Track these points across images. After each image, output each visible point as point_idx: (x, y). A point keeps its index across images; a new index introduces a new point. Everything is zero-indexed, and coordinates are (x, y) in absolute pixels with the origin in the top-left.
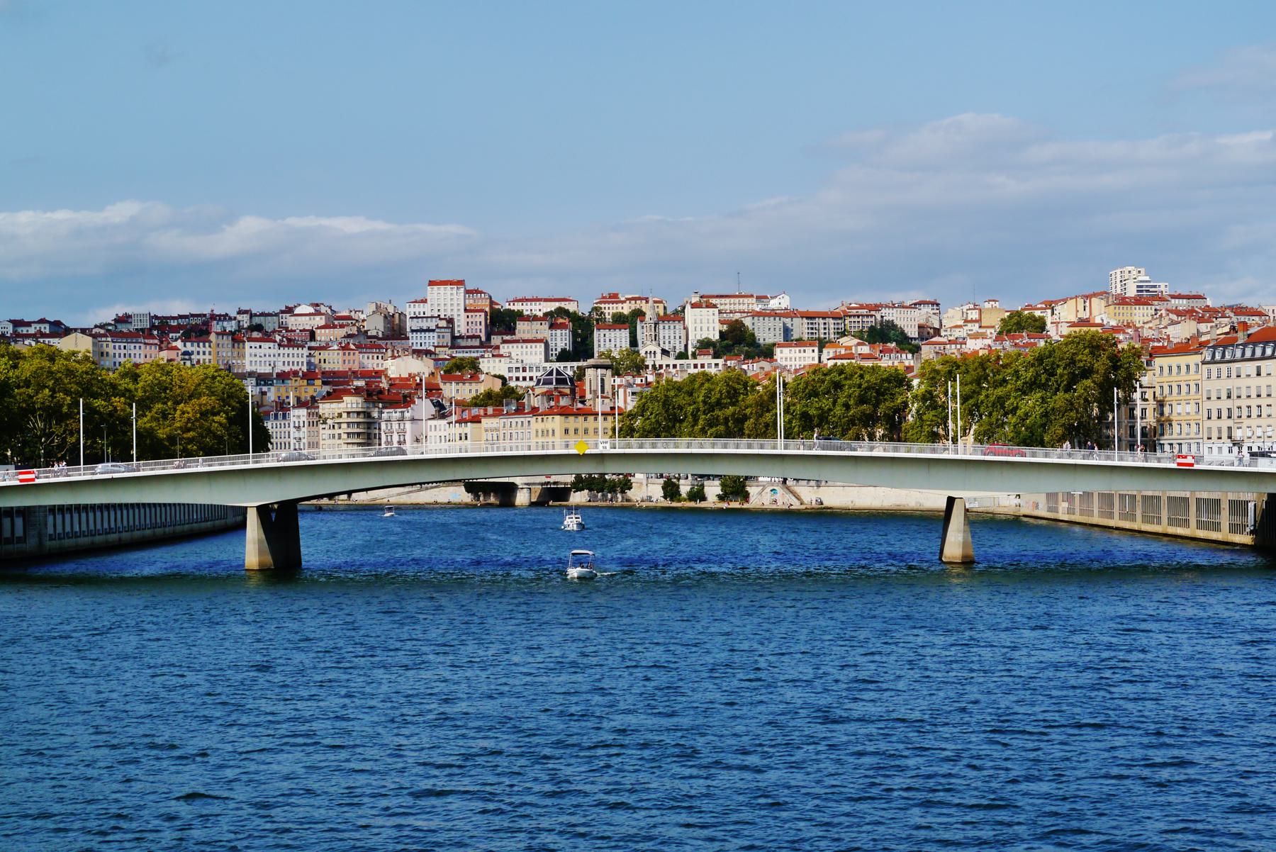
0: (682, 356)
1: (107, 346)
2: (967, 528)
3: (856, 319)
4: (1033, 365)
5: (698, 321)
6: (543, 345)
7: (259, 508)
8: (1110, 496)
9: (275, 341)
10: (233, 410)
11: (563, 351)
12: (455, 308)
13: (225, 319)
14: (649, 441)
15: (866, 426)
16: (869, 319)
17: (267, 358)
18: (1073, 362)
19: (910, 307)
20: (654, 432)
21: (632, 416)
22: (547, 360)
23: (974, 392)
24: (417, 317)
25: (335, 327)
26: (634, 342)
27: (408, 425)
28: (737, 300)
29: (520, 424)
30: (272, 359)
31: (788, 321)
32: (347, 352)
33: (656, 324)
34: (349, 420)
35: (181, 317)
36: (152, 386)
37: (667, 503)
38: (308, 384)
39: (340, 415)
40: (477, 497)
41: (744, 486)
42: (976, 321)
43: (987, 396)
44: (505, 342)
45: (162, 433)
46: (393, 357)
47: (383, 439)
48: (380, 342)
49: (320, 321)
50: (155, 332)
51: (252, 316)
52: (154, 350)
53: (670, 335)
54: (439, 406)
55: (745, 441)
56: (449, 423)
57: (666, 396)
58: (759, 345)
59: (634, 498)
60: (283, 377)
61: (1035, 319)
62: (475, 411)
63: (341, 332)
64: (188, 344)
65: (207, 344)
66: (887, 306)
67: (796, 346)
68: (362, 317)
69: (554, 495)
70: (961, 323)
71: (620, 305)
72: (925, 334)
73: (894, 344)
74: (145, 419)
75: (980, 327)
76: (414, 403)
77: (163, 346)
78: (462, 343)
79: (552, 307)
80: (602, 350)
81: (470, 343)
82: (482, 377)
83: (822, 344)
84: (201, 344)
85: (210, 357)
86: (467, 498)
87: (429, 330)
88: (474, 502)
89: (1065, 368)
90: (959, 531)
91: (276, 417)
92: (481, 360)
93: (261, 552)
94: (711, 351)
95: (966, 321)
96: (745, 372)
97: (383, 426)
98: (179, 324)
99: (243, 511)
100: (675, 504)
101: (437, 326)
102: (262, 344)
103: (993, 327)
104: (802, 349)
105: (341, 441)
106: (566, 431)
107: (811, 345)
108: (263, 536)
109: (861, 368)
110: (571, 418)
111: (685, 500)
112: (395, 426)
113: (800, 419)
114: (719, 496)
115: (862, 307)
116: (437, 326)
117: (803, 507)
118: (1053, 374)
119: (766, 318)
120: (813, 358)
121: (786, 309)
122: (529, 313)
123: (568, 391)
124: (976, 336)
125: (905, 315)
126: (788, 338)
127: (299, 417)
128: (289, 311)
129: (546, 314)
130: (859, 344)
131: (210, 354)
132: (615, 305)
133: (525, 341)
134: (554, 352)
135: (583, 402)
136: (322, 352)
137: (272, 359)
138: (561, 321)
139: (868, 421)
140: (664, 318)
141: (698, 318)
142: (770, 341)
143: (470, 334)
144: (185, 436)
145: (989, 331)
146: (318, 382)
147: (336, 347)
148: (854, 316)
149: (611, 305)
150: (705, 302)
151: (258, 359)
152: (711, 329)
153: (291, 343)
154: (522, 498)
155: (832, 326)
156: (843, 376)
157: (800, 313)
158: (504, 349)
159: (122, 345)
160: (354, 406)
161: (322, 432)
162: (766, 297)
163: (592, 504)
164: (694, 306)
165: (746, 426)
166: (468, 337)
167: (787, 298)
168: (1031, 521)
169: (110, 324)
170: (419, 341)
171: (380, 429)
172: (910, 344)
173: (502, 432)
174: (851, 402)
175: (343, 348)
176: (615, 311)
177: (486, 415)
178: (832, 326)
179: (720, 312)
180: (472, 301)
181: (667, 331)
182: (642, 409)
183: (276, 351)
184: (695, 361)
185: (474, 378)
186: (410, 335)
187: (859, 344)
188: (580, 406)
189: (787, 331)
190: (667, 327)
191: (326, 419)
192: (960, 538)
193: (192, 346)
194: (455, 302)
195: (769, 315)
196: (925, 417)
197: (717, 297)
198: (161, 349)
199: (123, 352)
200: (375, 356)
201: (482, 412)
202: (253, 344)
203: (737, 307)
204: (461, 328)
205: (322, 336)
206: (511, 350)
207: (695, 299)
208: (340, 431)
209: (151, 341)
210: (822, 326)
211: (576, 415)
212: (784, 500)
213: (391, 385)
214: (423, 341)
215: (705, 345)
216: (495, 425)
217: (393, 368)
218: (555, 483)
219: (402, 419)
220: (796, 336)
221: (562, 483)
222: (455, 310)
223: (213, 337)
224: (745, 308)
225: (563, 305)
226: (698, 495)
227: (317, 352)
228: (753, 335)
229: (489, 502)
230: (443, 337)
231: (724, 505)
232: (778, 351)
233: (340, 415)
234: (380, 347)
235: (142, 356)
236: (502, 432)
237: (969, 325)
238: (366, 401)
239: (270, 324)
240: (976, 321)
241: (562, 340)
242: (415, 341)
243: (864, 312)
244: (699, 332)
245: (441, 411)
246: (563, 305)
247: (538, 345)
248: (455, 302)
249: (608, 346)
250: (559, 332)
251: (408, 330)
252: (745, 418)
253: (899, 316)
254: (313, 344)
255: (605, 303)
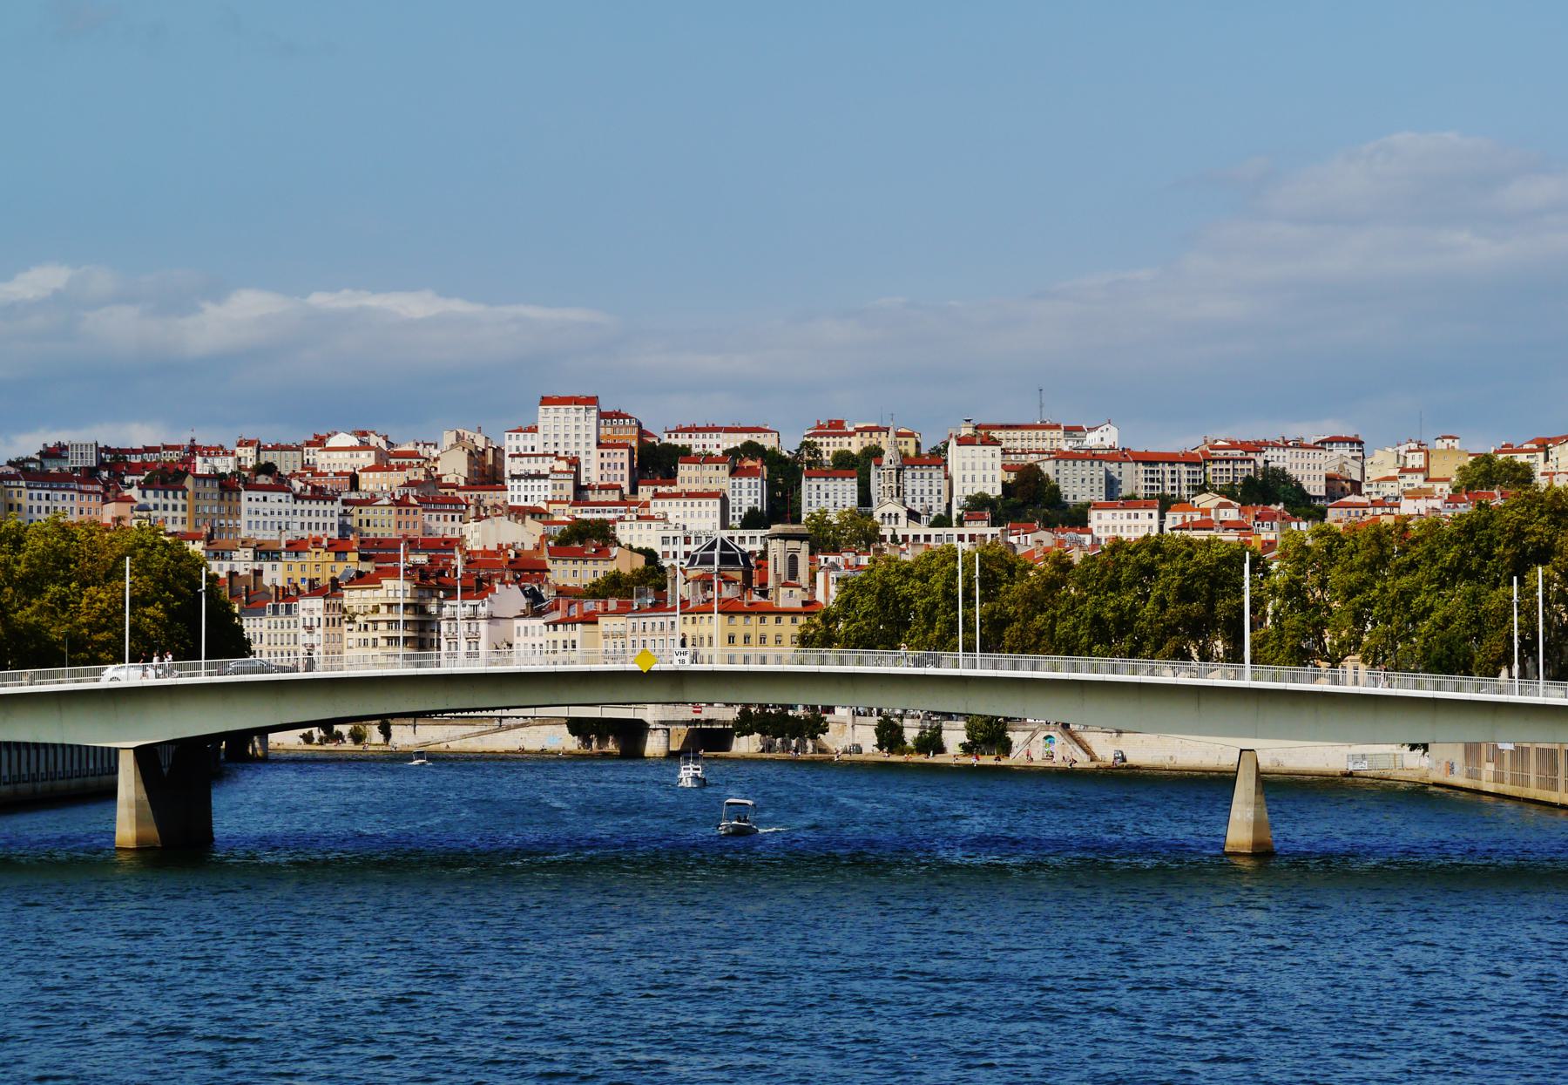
0: (942, 521)
1: (19, 494)
2: (1262, 799)
3: (1224, 466)
4: (1457, 541)
5: (969, 466)
6: (718, 502)
7: (137, 750)
8: (1552, 754)
9: (288, 491)
10: (175, 599)
11: (752, 511)
12: (582, 441)
13: (217, 454)
14: (849, 654)
15: (1194, 637)
16: (1246, 466)
17: (276, 518)
18: (1519, 534)
19: (1314, 447)
20: (865, 641)
21: (829, 618)
22: (725, 525)
23: (1364, 583)
24: (520, 456)
25: (390, 469)
26: (865, 498)
27: (483, 626)
28: (1033, 433)
29: (658, 626)
30: (284, 518)
31: (1113, 467)
32: (404, 509)
33: (899, 470)
34: (391, 617)
35: (147, 450)
36: (43, 558)
37: (883, 756)
38: (337, 560)
39: (376, 609)
40: (587, 741)
41: (1004, 730)
42: (1419, 470)
43: (1384, 590)
44: (657, 495)
45: (57, 632)
46: (478, 518)
47: (444, 644)
48: (461, 495)
49: (367, 458)
50: (105, 474)
51: (260, 449)
52: (95, 501)
53: (923, 487)
54: (534, 597)
55: (1005, 658)
56: (547, 624)
57: (882, 582)
58: (1066, 506)
59: (832, 748)
60: (296, 547)
61: (1517, 468)
62: (589, 605)
63: (398, 478)
64: (150, 493)
65: (180, 494)
66: (1275, 445)
67: (1124, 507)
68: (435, 453)
69: (706, 740)
70: (1395, 472)
71: (846, 440)
72: (1338, 489)
73: (1281, 506)
74: (29, 610)
75: (1426, 480)
76: (493, 591)
77: (109, 495)
78: (593, 497)
79: (737, 440)
80: (814, 510)
81: (604, 497)
82: (614, 551)
83: (1166, 504)
84: (170, 494)
85: (185, 514)
86: (571, 743)
87: (538, 476)
88: (583, 751)
89: (1507, 546)
90: (1248, 804)
91: (276, 611)
92: (618, 525)
93: (140, 821)
94: (988, 514)
95: (1404, 470)
96: (1013, 547)
97: (444, 627)
98: (144, 461)
99: (116, 752)
100: (895, 758)
101: (552, 471)
102: (268, 494)
103: (1447, 480)
104: (1133, 512)
105: (376, 651)
106: (731, 639)
107: (1146, 507)
108: (145, 796)
109: (1189, 543)
110: (740, 619)
111: (911, 751)
112: (463, 627)
113: (1092, 625)
114: (963, 746)
115: (1234, 446)
116: (552, 471)
117: (1093, 765)
118: (1489, 556)
119: (1079, 463)
120: (1150, 527)
121: (1112, 448)
122: (700, 450)
123: (738, 575)
124: (1415, 495)
125: (1305, 461)
126: (1113, 495)
127: (311, 610)
128: (320, 442)
129: (726, 453)
130: (1221, 505)
131: (184, 507)
132: (838, 440)
133: (690, 495)
134: (737, 514)
135: (764, 594)
136: (364, 509)
137: (284, 518)
138: (749, 463)
139: (1199, 628)
140: (906, 462)
141: (969, 462)
142: (1083, 499)
143: (605, 482)
144: (95, 637)
145: (1438, 486)
146: (352, 557)
147: (386, 501)
148: (1221, 460)
149: (831, 440)
150: (982, 436)
151: (261, 518)
152: (989, 479)
153: (319, 494)
154: (654, 745)
155: (1185, 476)
156: (1158, 556)
157: (1134, 454)
158: (657, 508)
159: (44, 493)
160: (400, 594)
161: (347, 635)
162: (1080, 429)
163: (766, 755)
164: (962, 441)
165: (1006, 633)
166: (601, 488)
167: (1113, 430)
168: (1452, 793)
169: (32, 460)
170: (523, 494)
171: (439, 632)
172: (1312, 507)
173: (630, 639)
174: (1170, 598)
175: (398, 503)
176: (837, 448)
177: (606, 612)
178: (1185, 476)
179: (1005, 452)
180: (609, 431)
181: (918, 482)
182: (847, 603)
183: (290, 506)
184: (961, 531)
185: (602, 554)
186: (509, 483)
187: (1221, 505)
188: (756, 598)
189: (1111, 484)
190: (918, 475)
191: (354, 615)
192: (1249, 813)
193: (156, 495)
194: (582, 432)
195: (1083, 458)
196: (1285, 623)
197: (1002, 427)
198: (106, 501)
199: (44, 504)
200: (450, 516)
201: (600, 607)
202: (253, 494)
203: (1034, 445)
204: (591, 473)
205: (369, 482)
206: (667, 509)
207: (966, 431)
208: (377, 635)
209: (90, 488)
210: (1168, 476)
211: (747, 614)
212: (1064, 754)
213: (468, 562)
214: (529, 494)
215: (978, 505)
216: (619, 628)
217: (477, 535)
218: (708, 722)
219: (473, 617)
220: (1125, 492)
221: (719, 722)
222: (583, 444)
223: (189, 482)
224: (1046, 445)
225: (754, 437)
226: (932, 743)
227: (356, 509)
228: (1057, 488)
229: (605, 750)
230: (562, 487)
231: (971, 760)
232: (1093, 515)
233: (376, 609)
234: (457, 502)
235: (76, 511)
236: (630, 639)
237: (1408, 476)
238: (419, 587)
239: (286, 463)
240: (1419, 470)
241: (749, 494)
242: (516, 493)
243: (1238, 453)
244: (969, 484)
245: (535, 607)
246: (754, 437)
247: (711, 501)
248: (582, 432)
249: (823, 504)
250: (745, 481)
251: (507, 475)
252: (1009, 621)
253: (1295, 461)
254: (354, 496)
255: (822, 435)
